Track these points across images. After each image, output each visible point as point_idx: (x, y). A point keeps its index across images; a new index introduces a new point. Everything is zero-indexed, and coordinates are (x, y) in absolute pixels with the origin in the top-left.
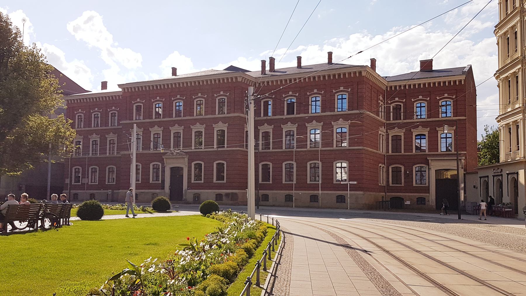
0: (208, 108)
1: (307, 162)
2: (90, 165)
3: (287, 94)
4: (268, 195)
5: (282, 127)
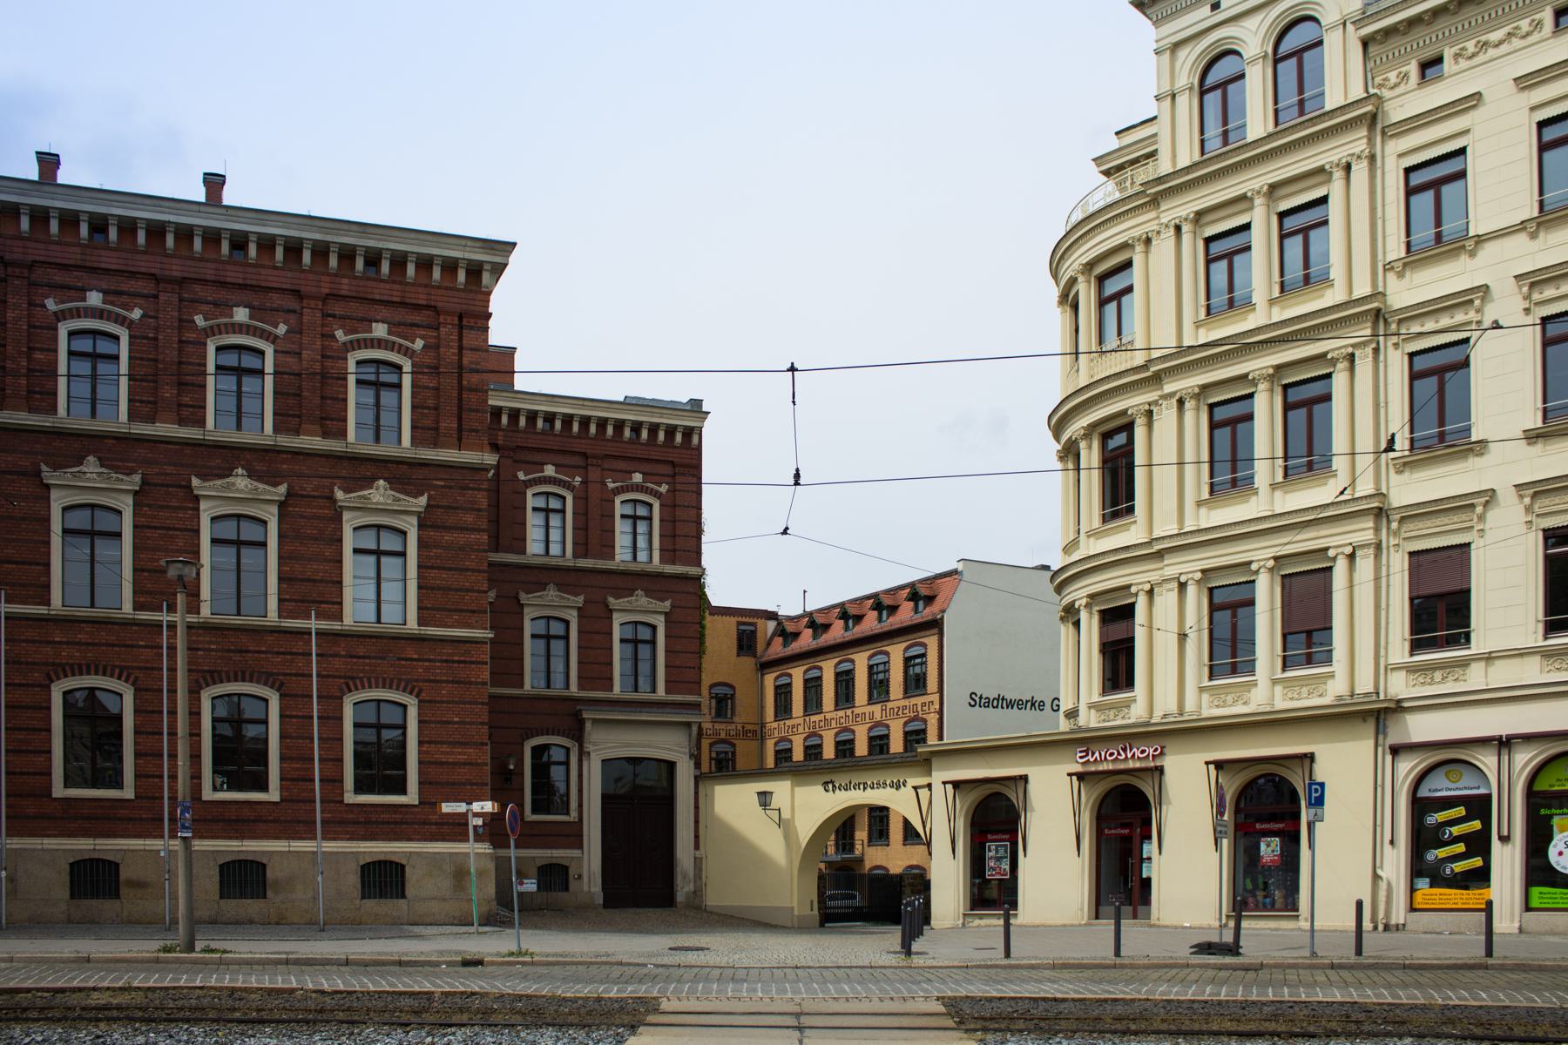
0: (299, 375)
1: (201, 688)
2: (201, 678)
3: (72, 301)
4: (563, 866)
5: (195, 492)
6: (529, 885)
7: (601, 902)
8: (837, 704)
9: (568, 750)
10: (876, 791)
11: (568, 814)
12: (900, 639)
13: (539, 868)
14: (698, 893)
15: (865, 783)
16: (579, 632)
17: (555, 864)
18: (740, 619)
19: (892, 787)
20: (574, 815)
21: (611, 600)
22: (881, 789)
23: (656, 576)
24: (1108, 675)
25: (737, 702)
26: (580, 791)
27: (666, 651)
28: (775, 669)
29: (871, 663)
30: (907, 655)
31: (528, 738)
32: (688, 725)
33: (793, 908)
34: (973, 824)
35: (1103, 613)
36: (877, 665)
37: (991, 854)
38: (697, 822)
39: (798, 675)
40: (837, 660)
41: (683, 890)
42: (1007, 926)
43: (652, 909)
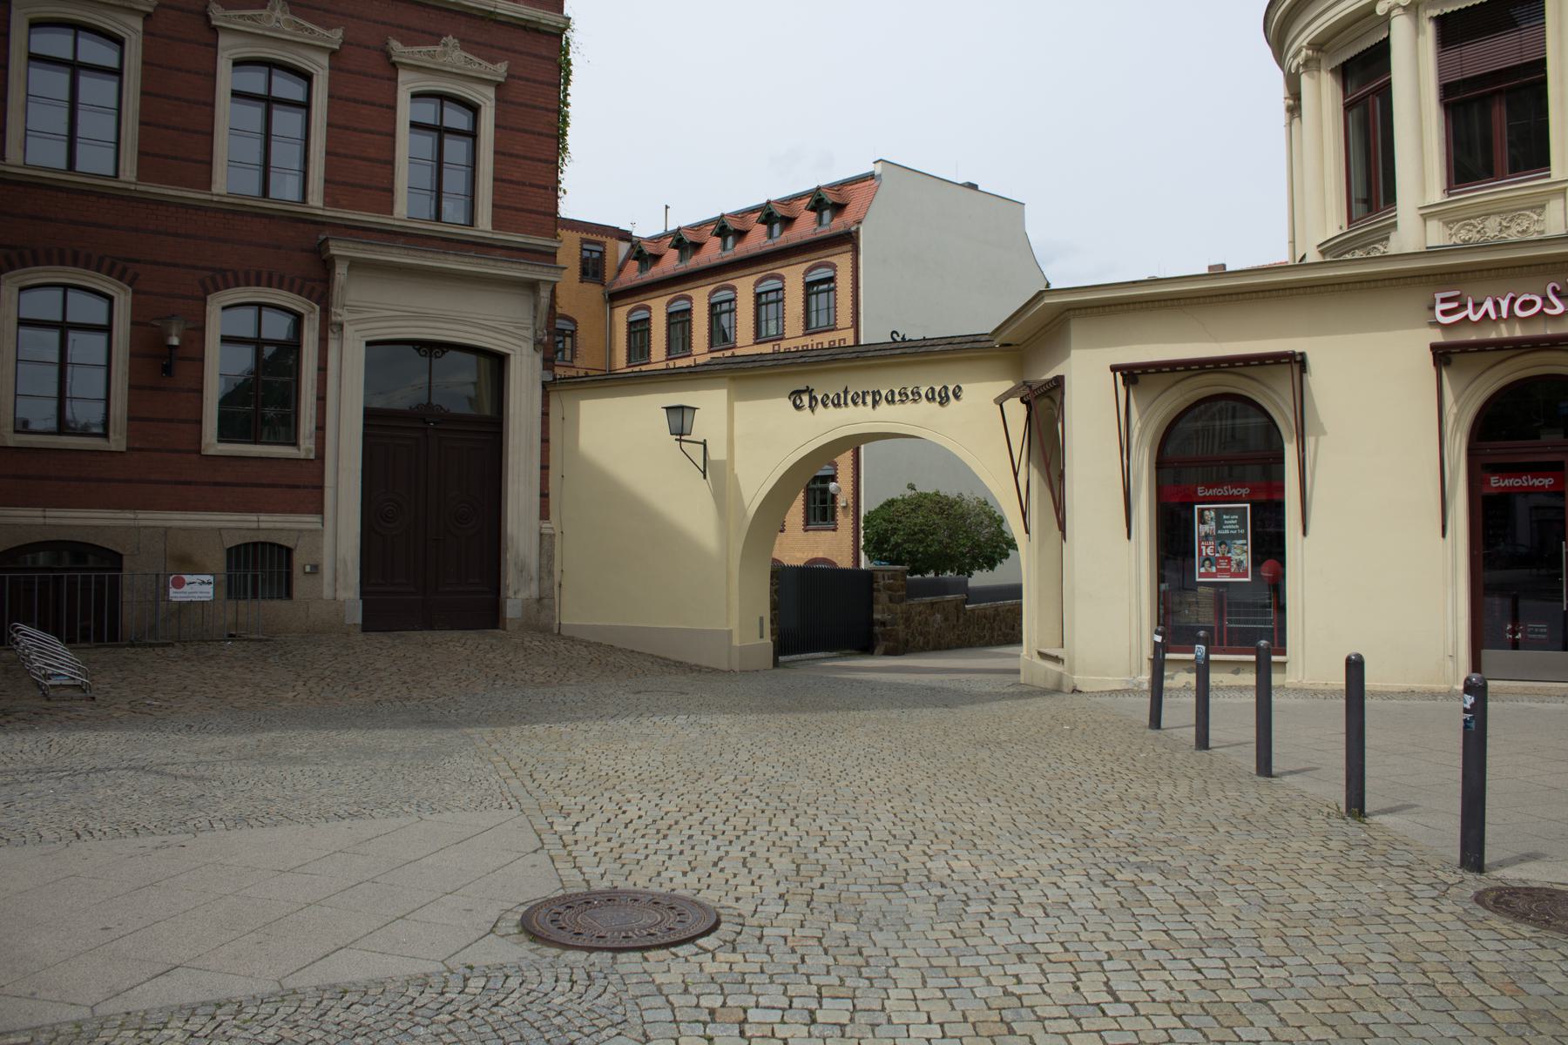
6: (196, 587)
7: (359, 619)
8: (711, 344)
9: (298, 319)
10: (898, 407)
11: (295, 443)
12: (800, 259)
13: (229, 550)
14: (544, 601)
15: (876, 393)
16: (331, 96)
17: (264, 544)
18: (584, 235)
19: (931, 399)
20: (306, 446)
21: (396, 46)
22: (909, 405)
23: (482, 18)
24: (1359, 192)
25: (579, 341)
26: (321, 399)
27: (496, 152)
28: (629, 300)
29: (758, 290)
30: (808, 279)
31: (217, 289)
32: (533, 286)
33: (730, 632)
34: (1162, 463)
35: (1442, 22)
36: (767, 292)
37: (1205, 529)
38: (545, 467)
39: (658, 308)
40: (711, 288)
41: (517, 595)
42: (1264, 691)
43: (457, 634)
